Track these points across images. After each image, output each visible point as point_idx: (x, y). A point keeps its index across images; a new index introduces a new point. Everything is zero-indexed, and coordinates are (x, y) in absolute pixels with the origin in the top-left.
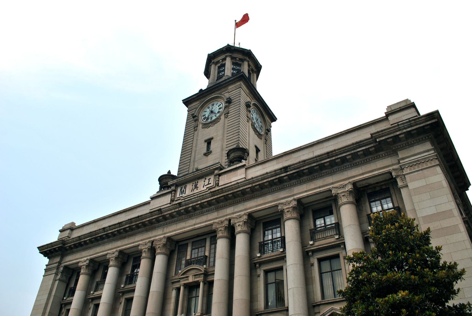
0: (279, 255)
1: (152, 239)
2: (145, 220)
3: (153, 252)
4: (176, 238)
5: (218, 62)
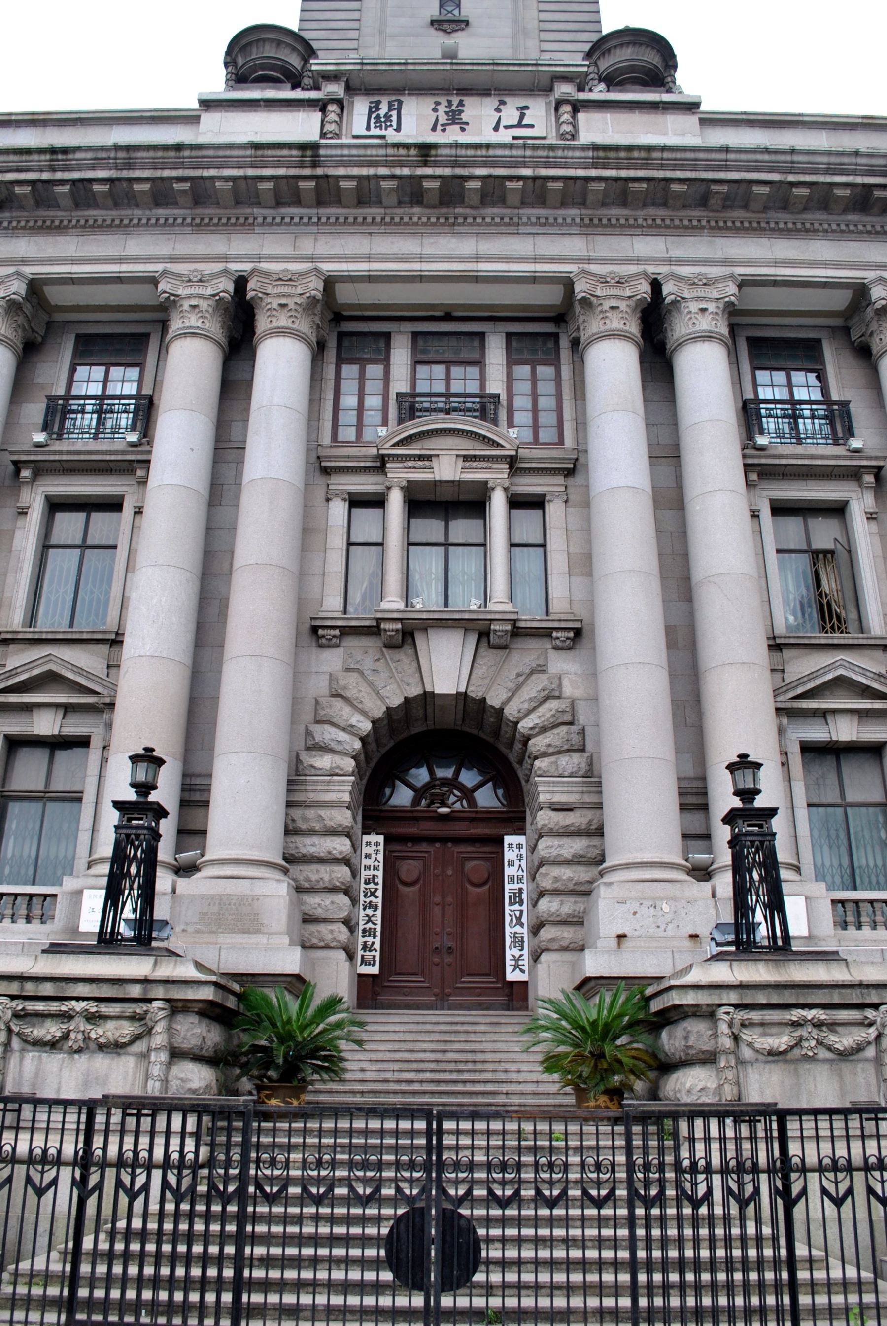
0: (123, 452)
3: (239, 330)
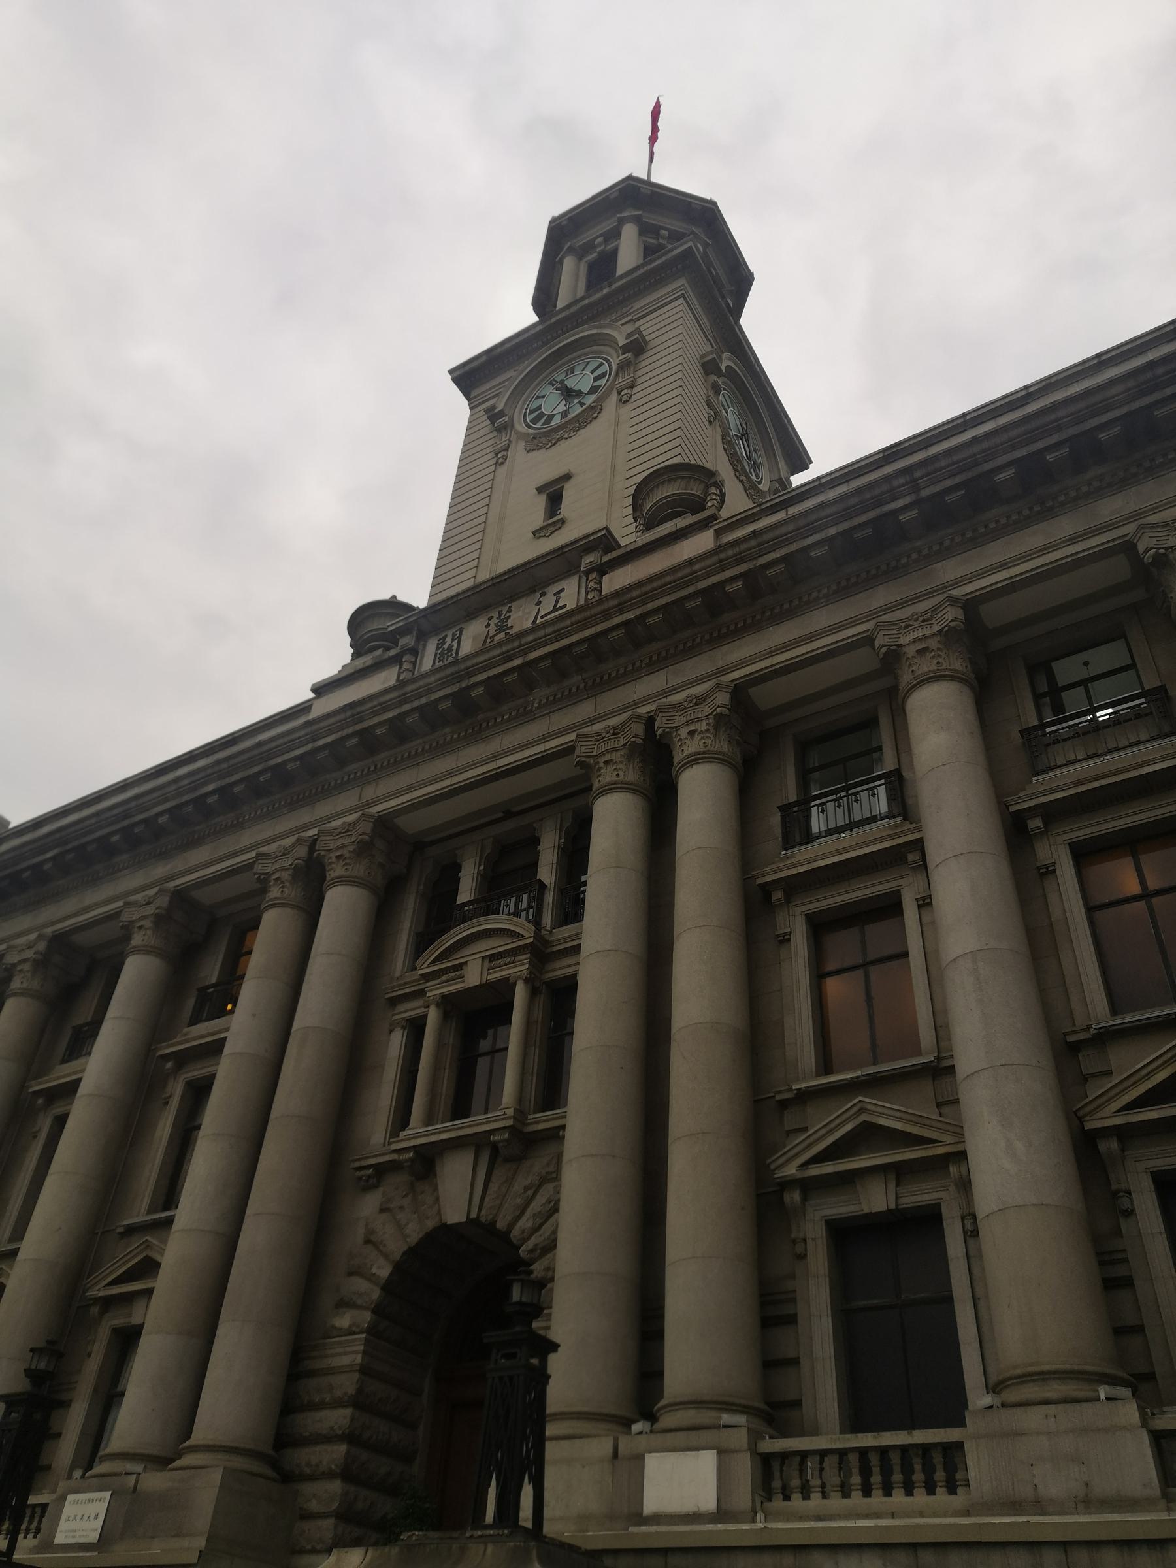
2: (286, 757)
3: (312, 879)
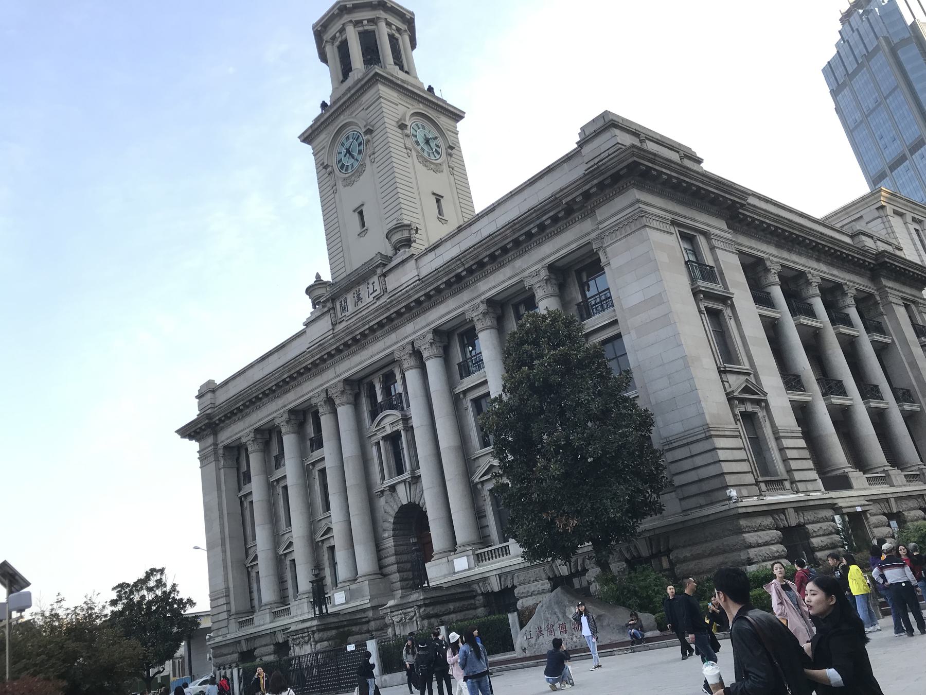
1: (325, 386)
4: (444, 328)
5: (334, 38)
